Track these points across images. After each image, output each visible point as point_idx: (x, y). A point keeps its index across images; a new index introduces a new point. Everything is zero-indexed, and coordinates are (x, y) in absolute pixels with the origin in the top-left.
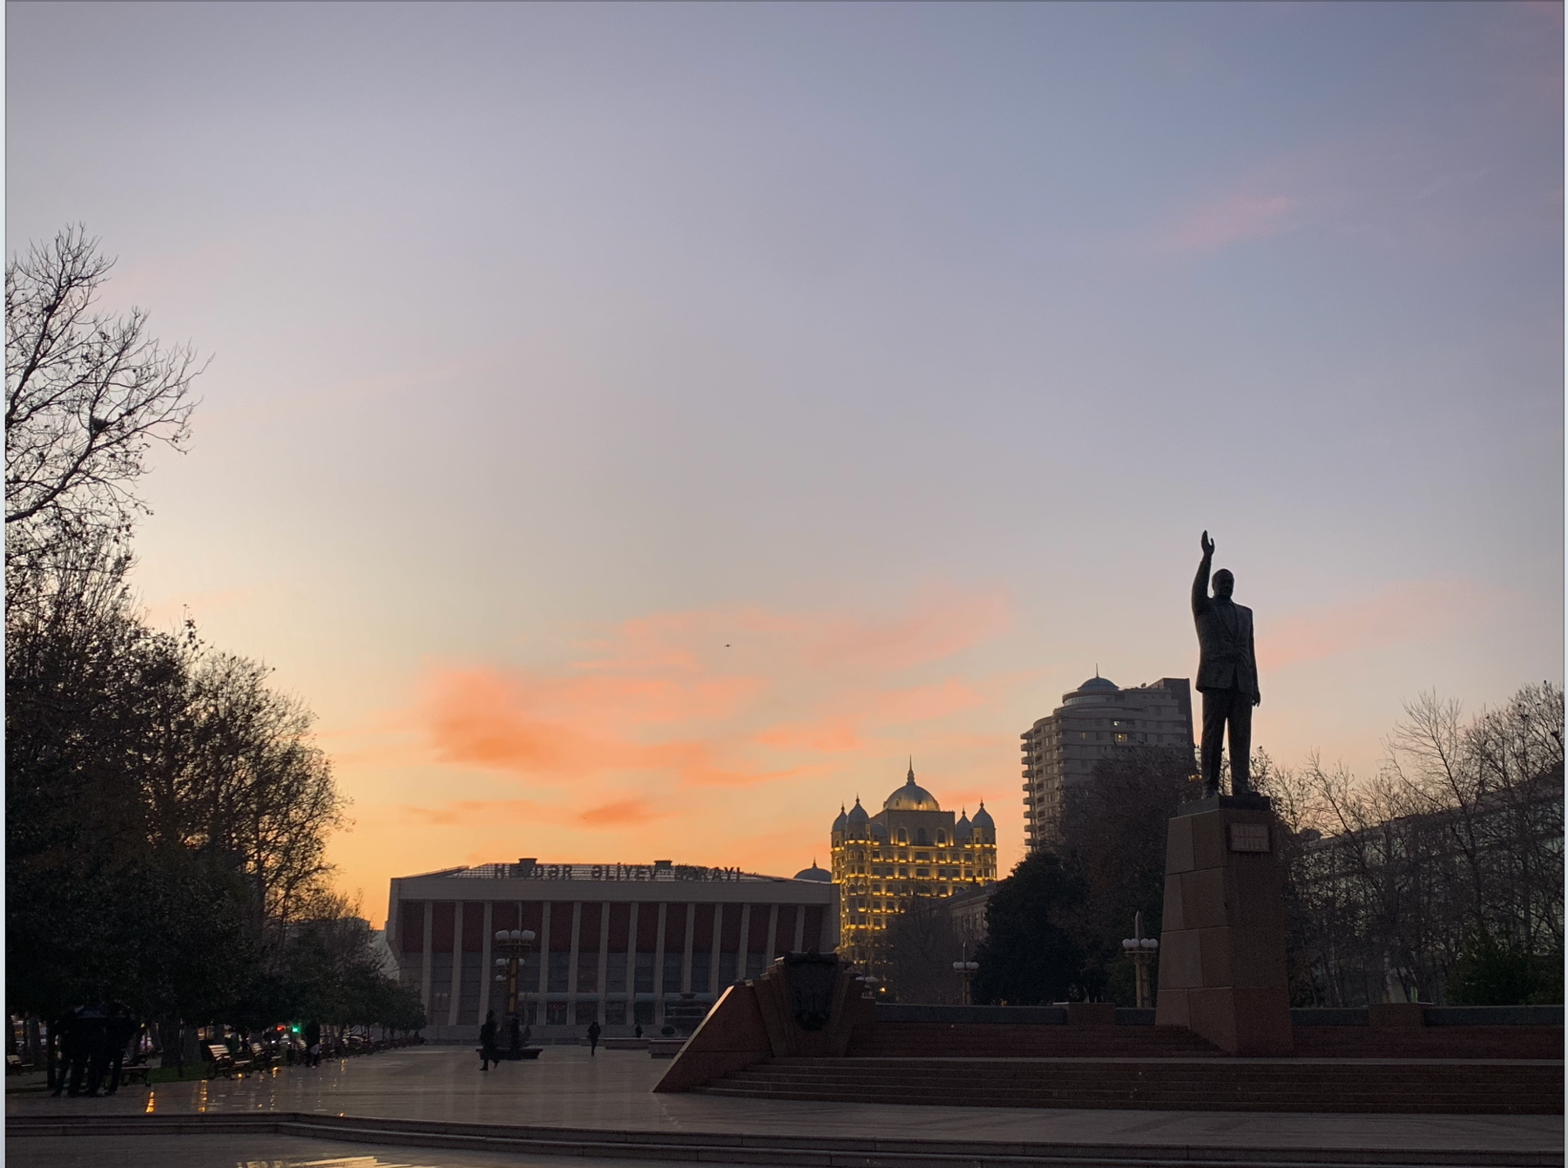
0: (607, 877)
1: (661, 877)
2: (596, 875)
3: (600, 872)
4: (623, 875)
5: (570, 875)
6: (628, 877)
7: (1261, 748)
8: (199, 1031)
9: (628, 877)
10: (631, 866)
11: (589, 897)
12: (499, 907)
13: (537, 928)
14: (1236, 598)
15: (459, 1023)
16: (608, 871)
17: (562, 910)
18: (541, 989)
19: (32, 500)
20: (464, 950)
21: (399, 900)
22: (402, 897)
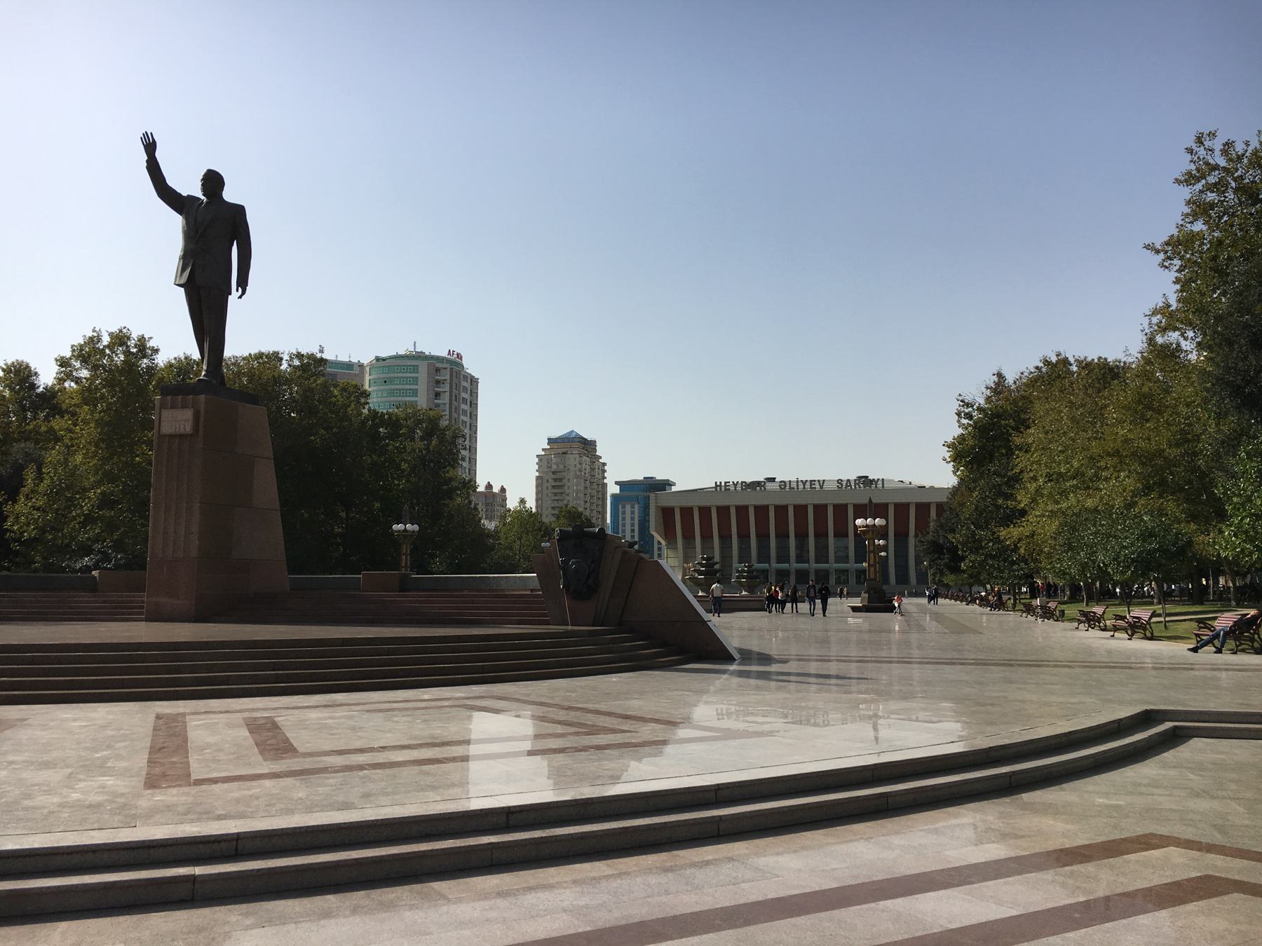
0: (790, 488)
1: (769, 486)
2: (783, 487)
3: (785, 485)
4: (801, 486)
5: (764, 488)
6: (804, 488)
7: (1165, 295)
8: (537, 585)
9: (804, 488)
10: (806, 481)
11: (779, 502)
12: (856, 507)
13: (886, 517)
14: (229, 195)
15: (897, 583)
16: (790, 485)
17: (902, 508)
18: (850, 561)
19: (1125, 412)
20: (739, 536)
21: (656, 506)
22: (658, 505)
